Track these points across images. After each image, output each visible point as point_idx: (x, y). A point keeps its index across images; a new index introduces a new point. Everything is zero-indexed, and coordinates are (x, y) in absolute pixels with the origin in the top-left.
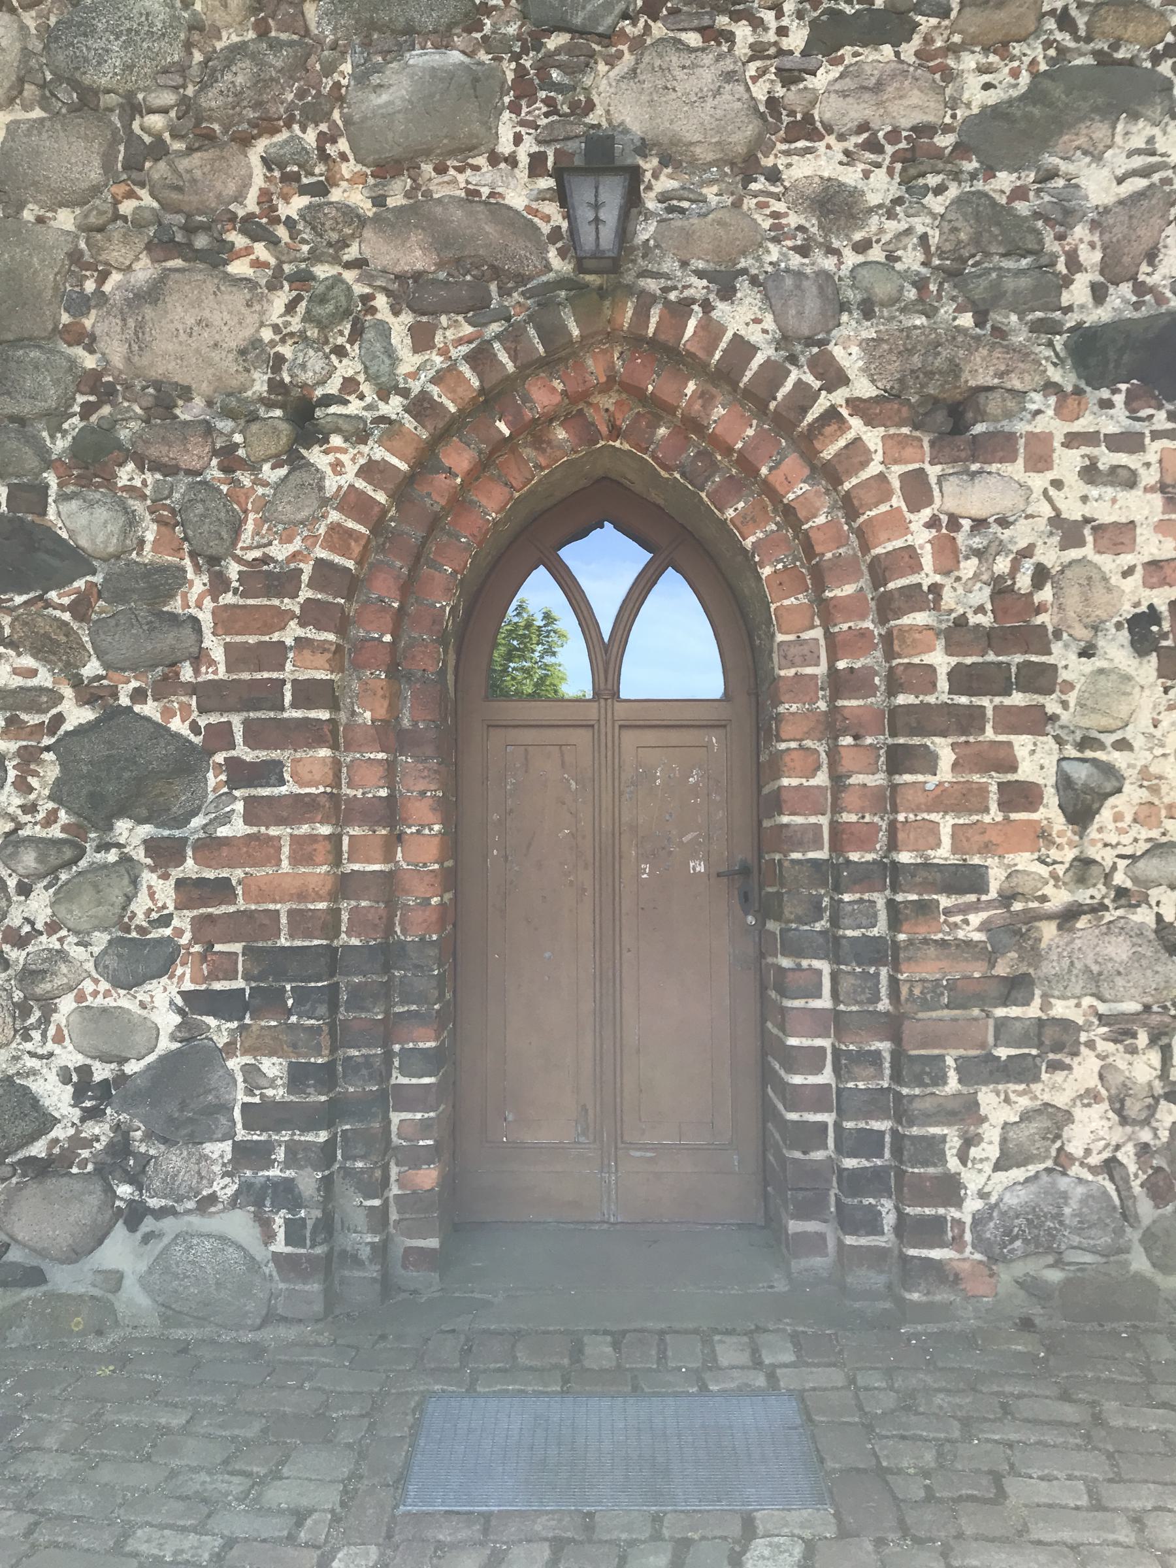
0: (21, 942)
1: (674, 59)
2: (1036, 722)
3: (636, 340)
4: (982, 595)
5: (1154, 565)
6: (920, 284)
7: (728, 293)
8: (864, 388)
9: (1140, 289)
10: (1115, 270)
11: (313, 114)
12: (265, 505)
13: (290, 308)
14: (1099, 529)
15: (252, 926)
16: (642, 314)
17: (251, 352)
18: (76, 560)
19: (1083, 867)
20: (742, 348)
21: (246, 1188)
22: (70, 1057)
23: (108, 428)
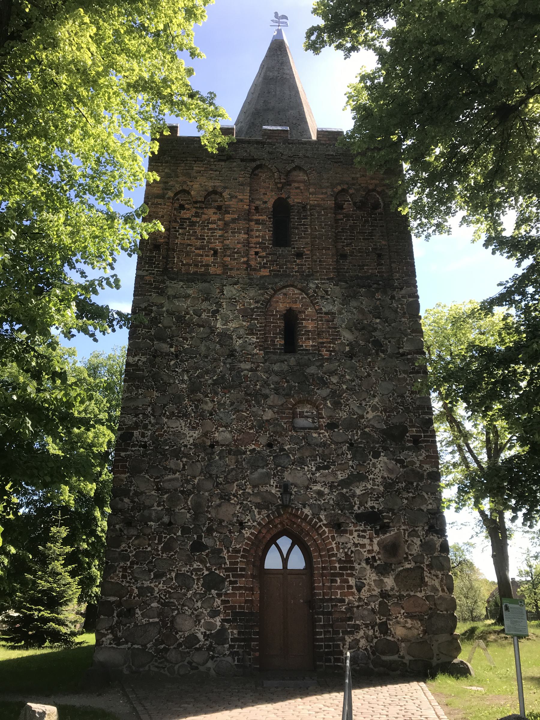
0: (196, 610)
1: (296, 471)
2: (352, 575)
3: (291, 514)
4: (343, 555)
5: (369, 551)
6: (333, 506)
7: (305, 507)
8: (325, 522)
9: (365, 507)
10: (361, 504)
11: (244, 479)
12: (236, 539)
13: (240, 508)
14: (360, 545)
15: (233, 608)
16: (292, 510)
17: (234, 515)
18: (206, 547)
19: (360, 599)
20: (307, 516)
21: (231, 652)
22: (203, 630)
23: (212, 526)
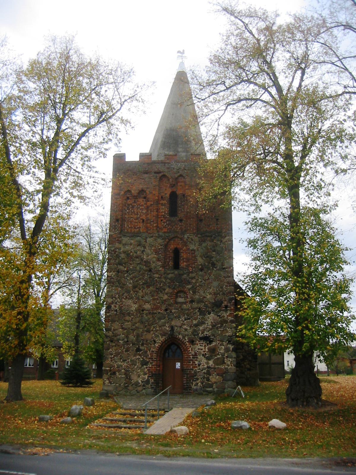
2: (196, 360)
15: (152, 372)
